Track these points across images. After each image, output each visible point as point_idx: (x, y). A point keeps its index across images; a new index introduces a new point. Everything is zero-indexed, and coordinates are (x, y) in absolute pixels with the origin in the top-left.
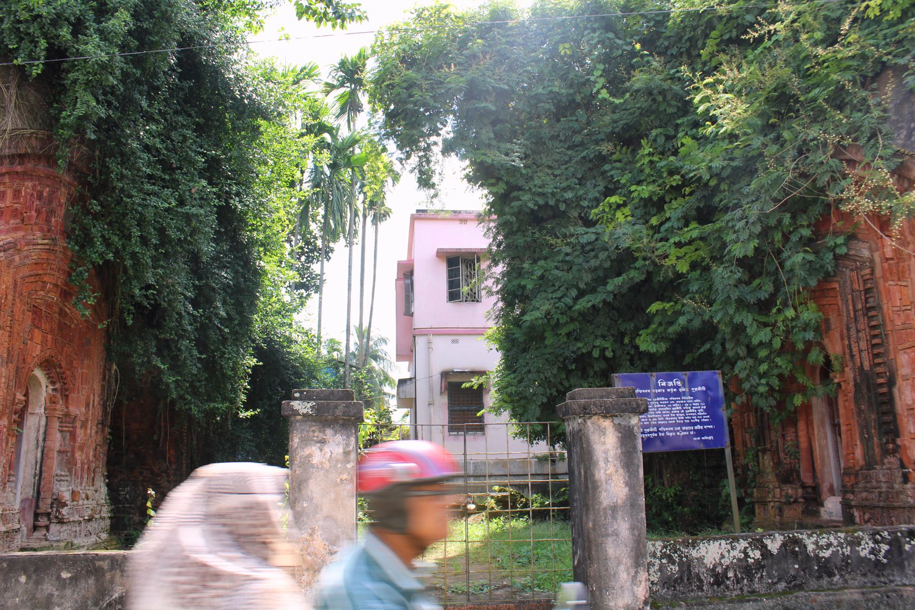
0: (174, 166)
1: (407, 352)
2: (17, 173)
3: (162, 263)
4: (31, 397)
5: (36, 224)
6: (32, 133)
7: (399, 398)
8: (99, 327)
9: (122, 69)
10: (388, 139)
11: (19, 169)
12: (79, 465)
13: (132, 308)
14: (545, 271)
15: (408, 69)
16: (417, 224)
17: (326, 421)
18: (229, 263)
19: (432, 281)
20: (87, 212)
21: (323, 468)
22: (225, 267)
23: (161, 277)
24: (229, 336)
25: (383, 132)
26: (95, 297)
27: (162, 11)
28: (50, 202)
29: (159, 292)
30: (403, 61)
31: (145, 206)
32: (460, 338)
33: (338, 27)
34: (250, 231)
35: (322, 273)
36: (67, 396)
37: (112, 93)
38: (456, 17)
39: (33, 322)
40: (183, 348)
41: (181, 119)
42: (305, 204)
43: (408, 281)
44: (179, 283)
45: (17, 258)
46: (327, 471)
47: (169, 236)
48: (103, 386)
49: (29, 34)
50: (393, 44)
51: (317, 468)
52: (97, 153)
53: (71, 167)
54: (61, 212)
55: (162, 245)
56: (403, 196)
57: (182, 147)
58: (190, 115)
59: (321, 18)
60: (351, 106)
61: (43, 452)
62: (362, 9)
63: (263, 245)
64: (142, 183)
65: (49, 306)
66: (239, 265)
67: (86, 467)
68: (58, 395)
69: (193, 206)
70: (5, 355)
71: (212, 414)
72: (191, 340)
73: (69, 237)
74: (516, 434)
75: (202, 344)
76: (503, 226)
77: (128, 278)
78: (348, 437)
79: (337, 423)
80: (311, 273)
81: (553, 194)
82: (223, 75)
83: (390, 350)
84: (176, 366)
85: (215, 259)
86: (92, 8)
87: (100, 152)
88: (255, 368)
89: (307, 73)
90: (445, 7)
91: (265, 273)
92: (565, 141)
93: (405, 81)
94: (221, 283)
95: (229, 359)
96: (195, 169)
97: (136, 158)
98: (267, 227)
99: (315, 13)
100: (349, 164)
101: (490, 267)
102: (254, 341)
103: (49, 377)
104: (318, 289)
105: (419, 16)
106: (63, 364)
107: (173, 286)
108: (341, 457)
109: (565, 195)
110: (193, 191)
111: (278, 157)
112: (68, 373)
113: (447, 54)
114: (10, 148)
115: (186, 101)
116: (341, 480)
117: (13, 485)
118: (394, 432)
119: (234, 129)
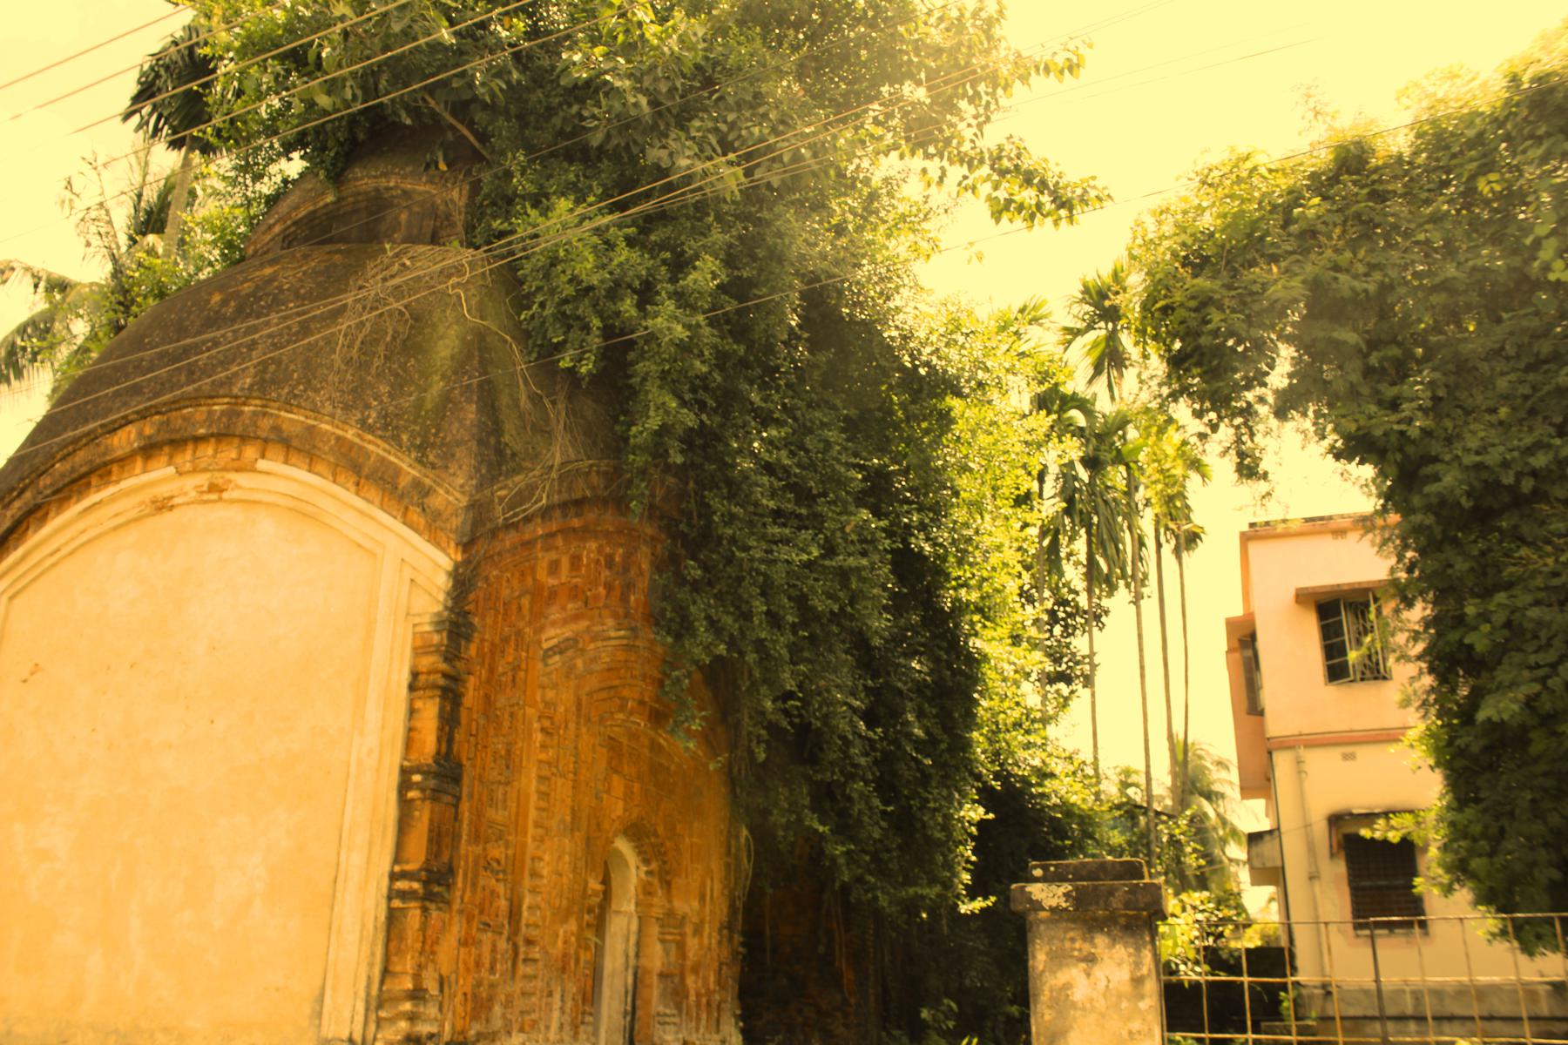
0: (815, 492)
1: (1259, 782)
2: (574, 530)
3: (806, 654)
4: (614, 884)
5: (606, 606)
6: (591, 466)
7: (1252, 869)
8: (711, 767)
9: (715, 347)
10: (1176, 401)
11: (576, 523)
12: (692, 998)
13: (763, 732)
14: (1513, 612)
15: (1195, 276)
16: (1253, 548)
17: (1095, 919)
18: (922, 645)
19: (1292, 649)
20: (681, 580)
21: (1093, 1009)
22: (916, 653)
23: (806, 677)
24: (933, 771)
25: (1165, 391)
26: (703, 718)
27: (768, 248)
28: (626, 569)
29: (806, 703)
30: (1185, 262)
31: (771, 563)
32: (1361, 751)
33: (1063, 223)
34: (955, 589)
35: (1092, 654)
36: (669, 883)
37: (706, 388)
38: (1270, 171)
39: (609, 763)
40: (855, 795)
41: (818, 414)
42: (1051, 531)
43: (1249, 653)
44: (837, 686)
45: (579, 663)
46: (1103, 1015)
47: (814, 608)
48: (728, 865)
49: (578, 318)
50: (1163, 237)
51: (1084, 1009)
52: (692, 484)
53: (652, 511)
54: (643, 584)
55: (805, 623)
56: (1218, 502)
57: (823, 460)
58: (834, 408)
59: (1033, 214)
60: (1111, 360)
61: (635, 974)
62: (1098, 183)
63: (979, 610)
64: (764, 525)
65: (633, 736)
66: (940, 648)
67: (704, 1000)
68: (656, 881)
69: (849, 555)
70: (568, 819)
71: (911, 907)
72: (867, 783)
73: (657, 624)
74: (1493, 935)
75: (887, 787)
76: (1411, 534)
77: (753, 684)
78: (1138, 949)
79: (1115, 923)
80: (1074, 654)
81: (1505, 464)
82: (880, 333)
83: (1227, 780)
84: (846, 828)
85: (896, 640)
86: (664, 262)
87: (696, 482)
88: (981, 824)
89: (1032, 315)
90: (1247, 158)
91: (986, 658)
92: (1518, 356)
93: (1193, 298)
94: (913, 680)
95: (935, 810)
96: (848, 493)
97: (750, 486)
98: (984, 580)
99: (1021, 208)
100: (1119, 459)
101: (1397, 611)
102: (978, 777)
103: (640, 851)
104: (1088, 681)
105: (1204, 183)
106: (660, 830)
107: (828, 691)
108: (1127, 988)
109: (1532, 460)
110: (848, 529)
111: (989, 458)
112: (668, 844)
113: (1262, 239)
114: (560, 492)
115: (825, 385)
116: (1130, 1032)
117: (590, 1029)
118: (1249, 931)
119: (908, 419)
